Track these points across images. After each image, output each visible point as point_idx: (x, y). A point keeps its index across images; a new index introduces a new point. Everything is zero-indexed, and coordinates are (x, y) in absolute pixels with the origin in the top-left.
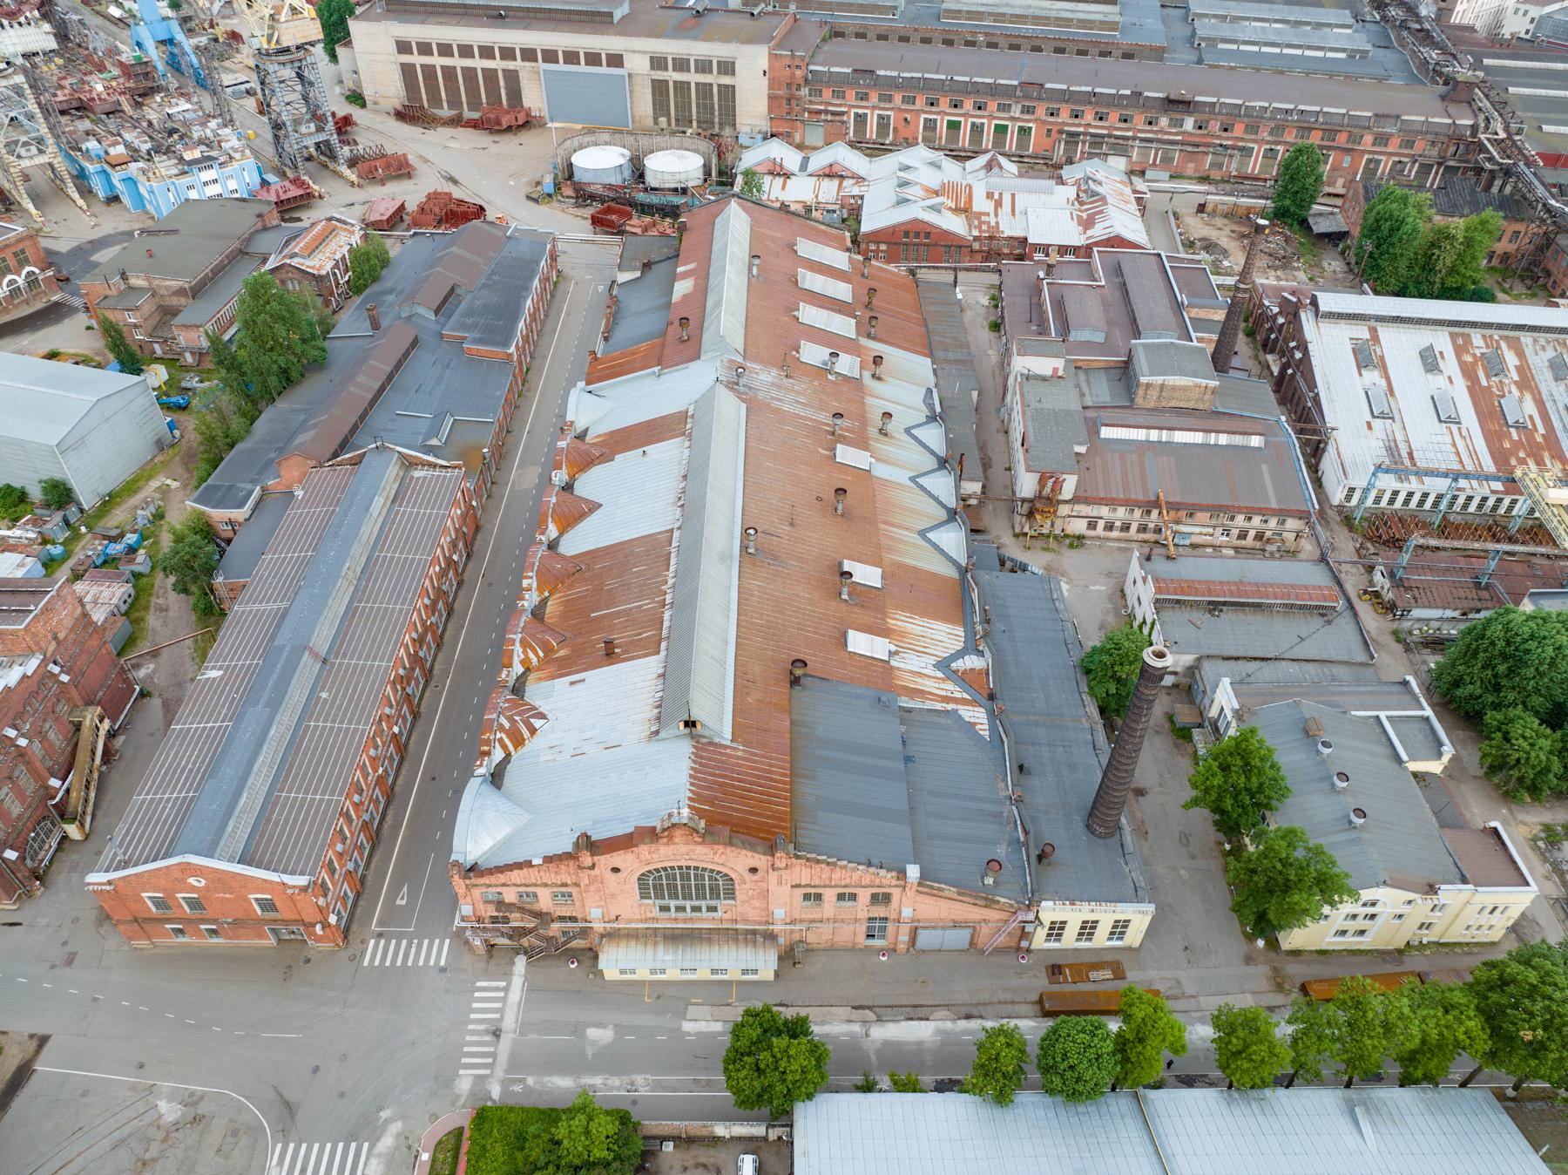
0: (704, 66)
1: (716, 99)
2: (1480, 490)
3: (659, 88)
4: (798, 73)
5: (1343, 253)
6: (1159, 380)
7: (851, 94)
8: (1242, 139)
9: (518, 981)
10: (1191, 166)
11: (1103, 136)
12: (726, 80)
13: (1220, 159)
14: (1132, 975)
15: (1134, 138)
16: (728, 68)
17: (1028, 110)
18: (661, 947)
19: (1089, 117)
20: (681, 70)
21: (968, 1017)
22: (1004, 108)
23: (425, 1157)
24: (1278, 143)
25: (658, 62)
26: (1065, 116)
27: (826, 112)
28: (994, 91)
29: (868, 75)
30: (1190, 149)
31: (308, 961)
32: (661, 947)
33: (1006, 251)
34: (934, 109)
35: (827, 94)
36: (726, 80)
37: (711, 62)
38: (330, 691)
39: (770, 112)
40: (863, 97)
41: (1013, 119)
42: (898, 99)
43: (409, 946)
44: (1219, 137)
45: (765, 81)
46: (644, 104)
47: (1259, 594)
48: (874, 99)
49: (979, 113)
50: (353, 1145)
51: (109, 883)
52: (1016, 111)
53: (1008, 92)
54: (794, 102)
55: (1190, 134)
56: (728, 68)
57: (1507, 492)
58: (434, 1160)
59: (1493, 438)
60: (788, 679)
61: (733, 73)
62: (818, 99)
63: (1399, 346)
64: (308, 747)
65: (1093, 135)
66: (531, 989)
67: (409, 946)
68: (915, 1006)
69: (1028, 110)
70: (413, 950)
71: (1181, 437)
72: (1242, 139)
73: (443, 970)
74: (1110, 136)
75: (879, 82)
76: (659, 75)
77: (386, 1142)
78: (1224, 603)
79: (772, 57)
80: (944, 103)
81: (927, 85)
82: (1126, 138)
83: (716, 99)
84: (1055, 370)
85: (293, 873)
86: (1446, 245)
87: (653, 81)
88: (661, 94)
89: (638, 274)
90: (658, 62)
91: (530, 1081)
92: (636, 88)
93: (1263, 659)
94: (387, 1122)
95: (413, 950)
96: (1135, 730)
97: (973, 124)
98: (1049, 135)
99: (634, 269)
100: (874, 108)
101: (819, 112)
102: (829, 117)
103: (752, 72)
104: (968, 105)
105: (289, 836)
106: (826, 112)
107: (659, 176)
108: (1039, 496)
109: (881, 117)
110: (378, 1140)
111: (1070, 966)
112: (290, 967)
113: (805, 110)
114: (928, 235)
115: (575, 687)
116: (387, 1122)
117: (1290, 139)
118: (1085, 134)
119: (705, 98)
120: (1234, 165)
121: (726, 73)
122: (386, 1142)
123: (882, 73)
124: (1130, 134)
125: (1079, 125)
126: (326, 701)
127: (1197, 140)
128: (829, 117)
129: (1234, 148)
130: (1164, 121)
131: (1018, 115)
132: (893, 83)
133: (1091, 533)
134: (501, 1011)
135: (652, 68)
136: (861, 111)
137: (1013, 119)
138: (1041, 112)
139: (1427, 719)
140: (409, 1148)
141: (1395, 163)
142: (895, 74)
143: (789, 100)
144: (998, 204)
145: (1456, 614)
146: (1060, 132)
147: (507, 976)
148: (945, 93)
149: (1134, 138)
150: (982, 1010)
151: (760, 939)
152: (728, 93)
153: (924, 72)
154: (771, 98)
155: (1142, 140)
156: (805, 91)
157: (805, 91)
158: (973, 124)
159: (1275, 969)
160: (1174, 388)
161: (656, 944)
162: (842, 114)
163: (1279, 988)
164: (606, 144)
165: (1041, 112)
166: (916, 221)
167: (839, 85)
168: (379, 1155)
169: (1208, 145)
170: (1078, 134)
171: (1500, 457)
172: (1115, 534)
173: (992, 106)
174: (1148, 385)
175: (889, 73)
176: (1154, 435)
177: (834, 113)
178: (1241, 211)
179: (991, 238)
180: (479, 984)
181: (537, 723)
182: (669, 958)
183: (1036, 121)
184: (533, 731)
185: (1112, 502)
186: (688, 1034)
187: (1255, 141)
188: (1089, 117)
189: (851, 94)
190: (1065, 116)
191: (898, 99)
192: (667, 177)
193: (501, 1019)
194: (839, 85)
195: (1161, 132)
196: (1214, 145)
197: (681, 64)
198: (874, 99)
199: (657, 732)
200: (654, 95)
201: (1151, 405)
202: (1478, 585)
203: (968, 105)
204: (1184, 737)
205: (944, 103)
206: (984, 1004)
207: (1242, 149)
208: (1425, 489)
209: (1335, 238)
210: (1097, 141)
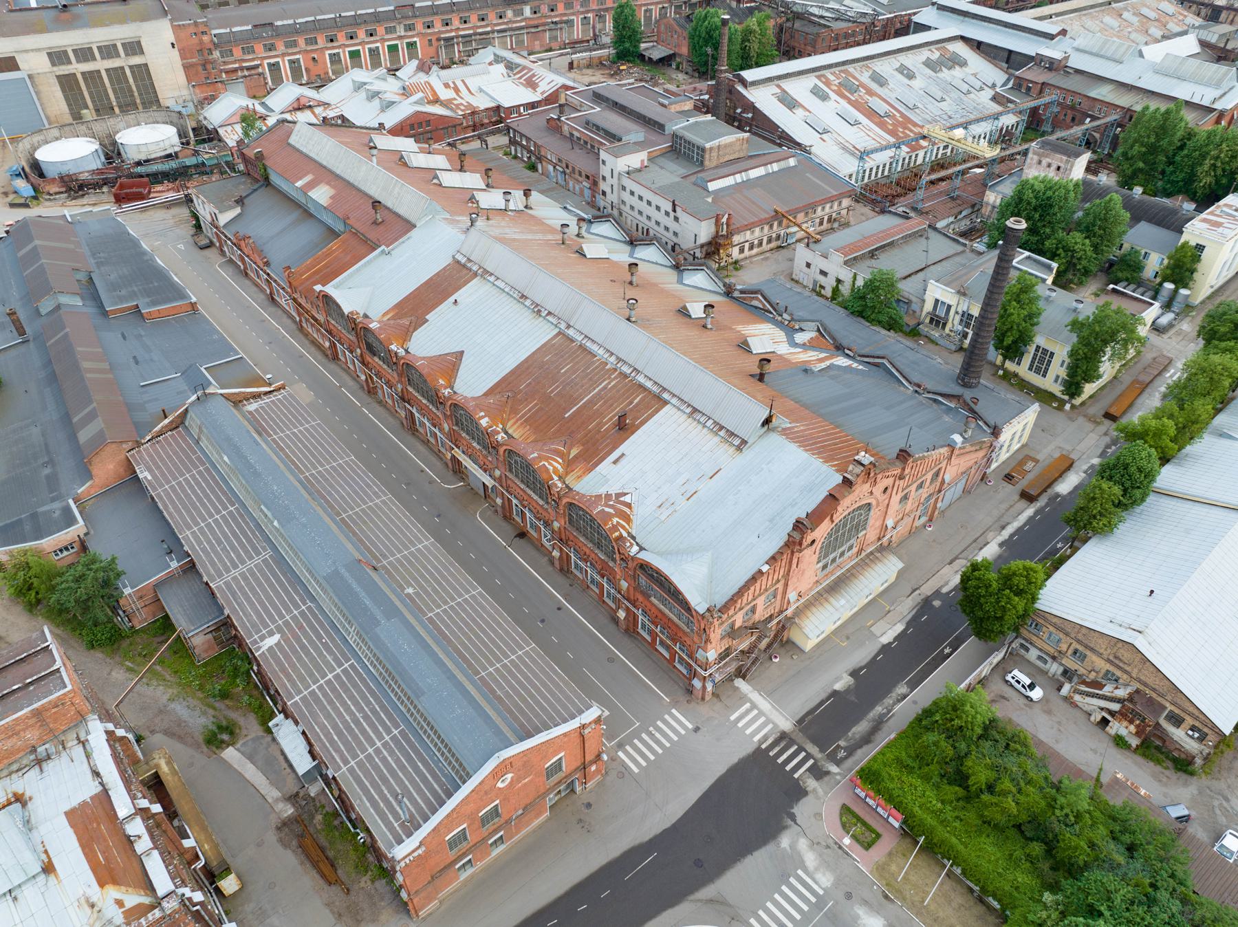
0: (109, 51)
1: (131, 80)
2: (883, 157)
3: (68, 83)
4: (205, 38)
5: (678, 68)
6: (715, 143)
7: (259, 48)
8: (565, 15)
9: (755, 696)
10: (537, 43)
11: (470, 35)
12: (136, 60)
13: (554, 33)
14: (1040, 457)
15: (493, 32)
16: (134, 47)
17: (410, 28)
18: (809, 614)
19: (456, 23)
20: (86, 60)
21: (1003, 528)
22: (390, 30)
23: (847, 841)
24: (588, 12)
25: (57, 57)
26: (438, 27)
27: (242, 69)
28: (377, 18)
29: (269, 28)
30: (533, 30)
31: (589, 805)
32: (832, 600)
33: (486, 121)
34: (335, 44)
35: (237, 52)
36: (136, 60)
37: (115, 46)
38: (410, 585)
39: (189, 81)
40: (271, 48)
41: (400, 38)
42: (301, 42)
43: (651, 735)
44: (550, 17)
45: (176, 52)
46: (57, 103)
47: (888, 236)
48: (281, 48)
49: (372, 39)
50: (792, 880)
51: (421, 844)
52: (401, 31)
53: (390, 16)
54: (209, 66)
55: (530, 19)
56: (134, 47)
57: (913, 151)
58: (854, 837)
59: (882, 125)
60: (755, 381)
61: (142, 52)
62: (232, 59)
63: (799, 89)
64: (452, 632)
65: (463, 36)
66: (769, 694)
67: (651, 735)
68: (975, 541)
69: (410, 28)
70: (658, 735)
71: (755, 173)
72: (565, 15)
73: (697, 729)
74: (475, 34)
75: (279, 32)
76: (64, 70)
77: (810, 859)
78: (876, 249)
79: (176, 29)
80: (342, 39)
81: (317, 26)
82: (487, 33)
83: (131, 80)
84: (642, 161)
85: (581, 712)
86: (752, 38)
87: (58, 77)
88: (71, 89)
89: (238, 210)
90: (57, 57)
91: (842, 743)
92: (41, 88)
93: (921, 270)
94: (793, 846)
95: (658, 735)
96: (1002, 288)
97: (370, 50)
98: (431, 45)
99: (231, 208)
100: (284, 55)
101: (235, 70)
102: (246, 73)
103: (160, 49)
104: (362, 35)
105: (532, 696)
106: (242, 69)
107: (143, 149)
108: (717, 235)
109: (292, 62)
110: (803, 862)
111: (1012, 470)
112: (580, 821)
113: (221, 71)
114: (428, 123)
115: (619, 465)
116: (793, 846)
117: (594, 7)
118: (457, 37)
119: (119, 82)
120: (565, 35)
121: (135, 54)
122: (810, 859)
123: (279, 23)
124: (489, 29)
125: (451, 31)
126: (417, 594)
127: (536, 22)
128: (246, 73)
129: (561, 22)
130: (510, 13)
131: (403, 33)
132: (295, 30)
133: (742, 256)
134: (768, 721)
135: (53, 64)
136: (272, 61)
137: (400, 38)
138: (419, 27)
139: (1028, 258)
140: (828, 847)
141: (646, 11)
142: (291, 22)
143: (204, 65)
144: (457, 90)
145: (951, 219)
146: (439, 40)
147: (743, 699)
148: (340, 28)
149: (493, 32)
150: (1005, 519)
151: (878, 555)
152: (143, 72)
153: (315, 15)
154: (186, 68)
155: (499, 31)
156: (216, 54)
157: (216, 54)
158: (370, 50)
159: (1085, 416)
160: (726, 146)
161: (827, 600)
162: (256, 67)
163: (1098, 424)
164: (57, 139)
165: (419, 27)
166: (418, 113)
167: (246, 42)
168: (817, 869)
169: (544, 24)
170: (452, 38)
171: (892, 133)
172: (755, 251)
173: (381, 30)
174: (711, 149)
175: (285, 22)
176: (738, 178)
177: (248, 69)
178: (595, 62)
179: (473, 113)
180: (732, 718)
181: (627, 499)
182: (843, 602)
183: (417, 35)
184: (629, 506)
185: (750, 227)
186: (890, 644)
187: (573, 14)
188: (456, 23)
189: (259, 48)
190: (438, 27)
191: (301, 42)
192: (152, 148)
193: (775, 725)
194: (246, 42)
195: (511, 22)
196: (547, 24)
197: (84, 54)
198: (281, 48)
199: (767, 421)
200: (63, 91)
201: (714, 164)
202: (952, 198)
203: (362, 35)
204: (915, 335)
205: (342, 39)
206: (1002, 516)
207: (567, 22)
208: (877, 163)
209: (666, 61)
210: (467, 39)
